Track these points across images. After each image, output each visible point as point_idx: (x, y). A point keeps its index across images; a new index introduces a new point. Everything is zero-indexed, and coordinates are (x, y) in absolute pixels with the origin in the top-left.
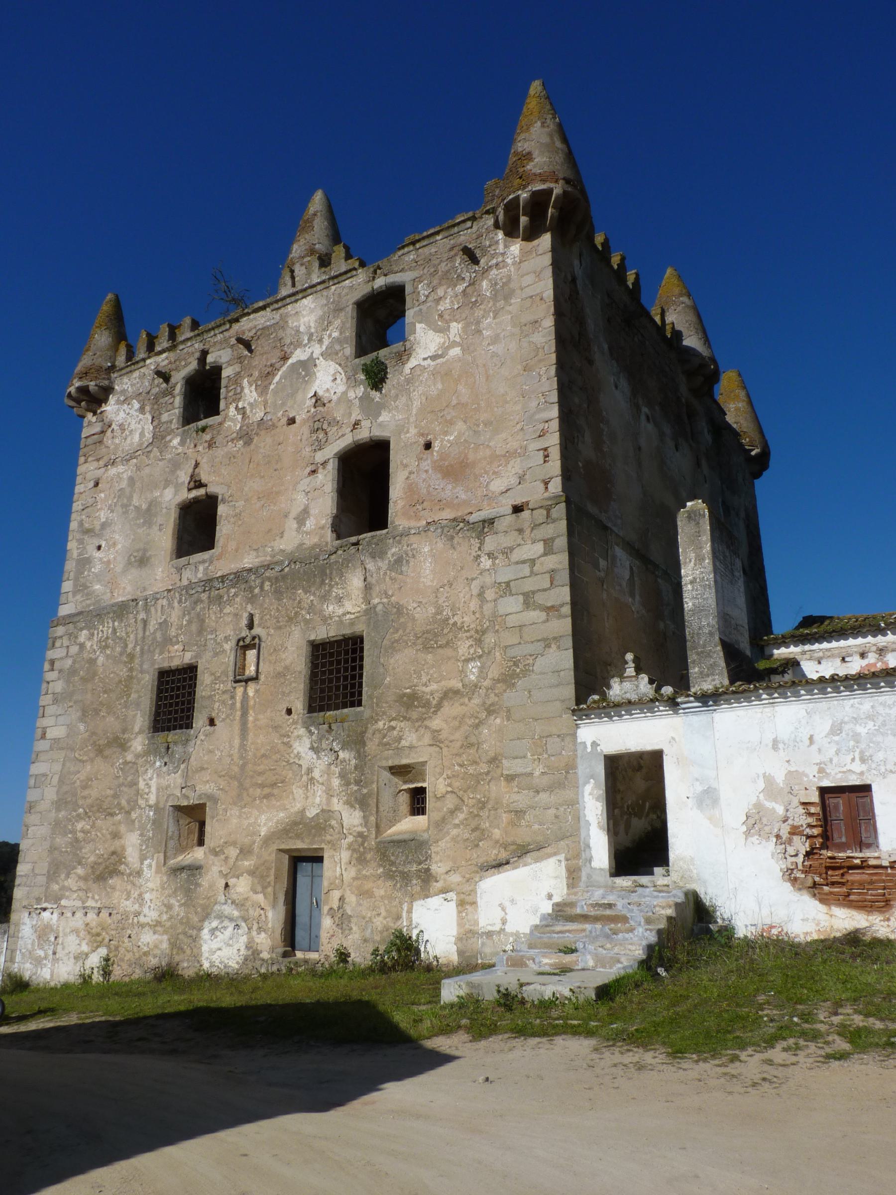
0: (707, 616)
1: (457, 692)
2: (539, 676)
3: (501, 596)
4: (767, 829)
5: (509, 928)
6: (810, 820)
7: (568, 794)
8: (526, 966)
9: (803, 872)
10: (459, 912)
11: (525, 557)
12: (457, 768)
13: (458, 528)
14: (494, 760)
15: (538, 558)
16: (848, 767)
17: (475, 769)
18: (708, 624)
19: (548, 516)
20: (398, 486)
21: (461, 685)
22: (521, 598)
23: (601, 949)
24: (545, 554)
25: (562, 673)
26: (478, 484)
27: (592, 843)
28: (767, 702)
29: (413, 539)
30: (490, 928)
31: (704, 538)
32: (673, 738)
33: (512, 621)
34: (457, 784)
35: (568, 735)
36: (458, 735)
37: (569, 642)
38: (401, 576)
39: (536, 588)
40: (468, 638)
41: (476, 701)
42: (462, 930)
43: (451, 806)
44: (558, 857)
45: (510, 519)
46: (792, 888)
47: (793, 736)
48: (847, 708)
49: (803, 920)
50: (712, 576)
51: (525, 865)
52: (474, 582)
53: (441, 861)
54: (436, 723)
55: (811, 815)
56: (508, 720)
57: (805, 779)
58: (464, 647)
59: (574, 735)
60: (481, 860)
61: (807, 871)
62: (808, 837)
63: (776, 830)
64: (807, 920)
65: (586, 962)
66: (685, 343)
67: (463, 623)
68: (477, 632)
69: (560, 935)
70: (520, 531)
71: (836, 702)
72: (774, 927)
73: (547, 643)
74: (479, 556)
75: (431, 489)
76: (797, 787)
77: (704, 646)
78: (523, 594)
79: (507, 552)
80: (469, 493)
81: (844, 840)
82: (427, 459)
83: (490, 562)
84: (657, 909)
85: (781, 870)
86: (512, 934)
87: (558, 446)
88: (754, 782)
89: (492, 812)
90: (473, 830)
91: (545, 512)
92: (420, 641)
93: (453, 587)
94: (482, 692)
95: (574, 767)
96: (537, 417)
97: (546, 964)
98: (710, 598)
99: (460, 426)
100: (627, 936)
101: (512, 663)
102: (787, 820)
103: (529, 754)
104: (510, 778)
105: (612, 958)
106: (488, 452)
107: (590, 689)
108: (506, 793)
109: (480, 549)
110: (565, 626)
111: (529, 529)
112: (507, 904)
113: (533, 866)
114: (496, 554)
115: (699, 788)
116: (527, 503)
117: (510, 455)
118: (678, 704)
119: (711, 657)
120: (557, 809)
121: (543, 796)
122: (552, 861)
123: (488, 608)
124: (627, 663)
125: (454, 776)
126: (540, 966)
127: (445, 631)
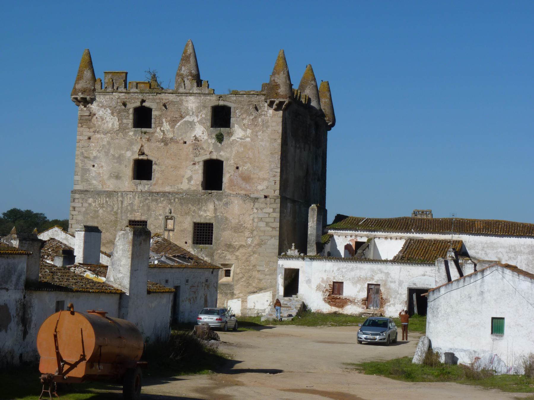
1: (244, 246)
11: (267, 212)
14: (254, 266)
24: (273, 212)
33: (262, 229)
41: (250, 249)
54: (237, 253)
58: (247, 234)
59: (277, 262)
70: (266, 204)
73: (272, 237)
79: (262, 209)
94: (252, 247)
98: (315, 232)
104: (259, 271)
106: (257, 176)
107: (282, 252)
110: (277, 233)
112: (256, 302)
115: (307, 279)
117: (264, 179)
121: (268, 277)
123: (255, 224)
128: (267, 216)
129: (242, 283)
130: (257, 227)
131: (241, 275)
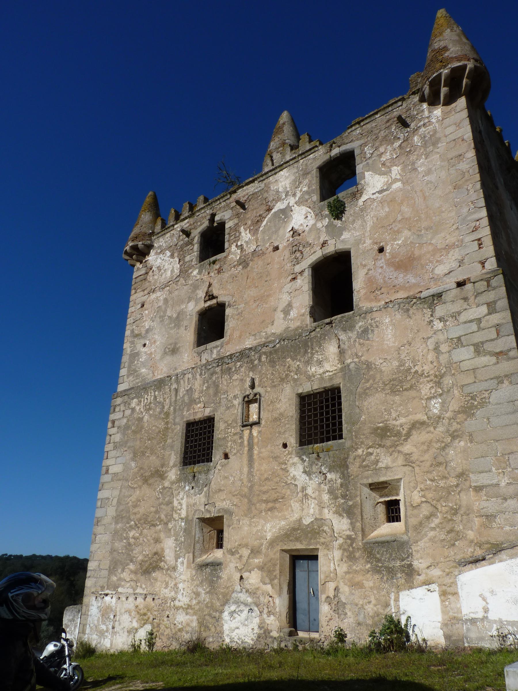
1: (423, 423)
2: (496, 406)
3: (454, 348)
5: (492, 616)
10: (442, 601)
11: (472, 317)
12: (428, 482)
13: (412, 303)
14: (461, 475)
19: (488, 286)
20: (359, 280)
21: (426, 417)
22: (472, 348)
24: (489, 314)
26: (425, 271)
29: (375, 315)
33: (465, 366)
34: (430, 495)
36: (427, 457)
38: (368, 342)
39: (485, 339)
40: (428, 382)
41: (441, 429)
42: (446, 617)
43: (426, 513)
51: (501, 561)
53: (422, 558)
54: (407, 448)
56: (471, 442)
58: (426, 389)
60: (458, 558)
67: (423, 371)
68: (436, 376)
70: (465, 299)
75: (386, 279)
78: (474, 345)
79: (455, 316)
80: (418, 278)
82: (381, 259)
86: (495, 622)
89: (465, 517)
90: (449, 532)
91: (485, 283)
92: (387, 387)
93: (412, 345)
94: (446, 421)
96: (469, 218)
99: (406, 233)
101: (470, 398)
103: (494, 469)
104: (478, 489)
106: (431, 248)
108: (476, 501)
109: (432, 315)
111: (473, 297)
112: (487, 595)
113: (509, 562)
116: (469, 279)
117: (448, 248)
123: (444, 359)
125: (427, 489)
127: (409, 378)
128: (474, 327)
130: (450, 364)
131: (426, 510)
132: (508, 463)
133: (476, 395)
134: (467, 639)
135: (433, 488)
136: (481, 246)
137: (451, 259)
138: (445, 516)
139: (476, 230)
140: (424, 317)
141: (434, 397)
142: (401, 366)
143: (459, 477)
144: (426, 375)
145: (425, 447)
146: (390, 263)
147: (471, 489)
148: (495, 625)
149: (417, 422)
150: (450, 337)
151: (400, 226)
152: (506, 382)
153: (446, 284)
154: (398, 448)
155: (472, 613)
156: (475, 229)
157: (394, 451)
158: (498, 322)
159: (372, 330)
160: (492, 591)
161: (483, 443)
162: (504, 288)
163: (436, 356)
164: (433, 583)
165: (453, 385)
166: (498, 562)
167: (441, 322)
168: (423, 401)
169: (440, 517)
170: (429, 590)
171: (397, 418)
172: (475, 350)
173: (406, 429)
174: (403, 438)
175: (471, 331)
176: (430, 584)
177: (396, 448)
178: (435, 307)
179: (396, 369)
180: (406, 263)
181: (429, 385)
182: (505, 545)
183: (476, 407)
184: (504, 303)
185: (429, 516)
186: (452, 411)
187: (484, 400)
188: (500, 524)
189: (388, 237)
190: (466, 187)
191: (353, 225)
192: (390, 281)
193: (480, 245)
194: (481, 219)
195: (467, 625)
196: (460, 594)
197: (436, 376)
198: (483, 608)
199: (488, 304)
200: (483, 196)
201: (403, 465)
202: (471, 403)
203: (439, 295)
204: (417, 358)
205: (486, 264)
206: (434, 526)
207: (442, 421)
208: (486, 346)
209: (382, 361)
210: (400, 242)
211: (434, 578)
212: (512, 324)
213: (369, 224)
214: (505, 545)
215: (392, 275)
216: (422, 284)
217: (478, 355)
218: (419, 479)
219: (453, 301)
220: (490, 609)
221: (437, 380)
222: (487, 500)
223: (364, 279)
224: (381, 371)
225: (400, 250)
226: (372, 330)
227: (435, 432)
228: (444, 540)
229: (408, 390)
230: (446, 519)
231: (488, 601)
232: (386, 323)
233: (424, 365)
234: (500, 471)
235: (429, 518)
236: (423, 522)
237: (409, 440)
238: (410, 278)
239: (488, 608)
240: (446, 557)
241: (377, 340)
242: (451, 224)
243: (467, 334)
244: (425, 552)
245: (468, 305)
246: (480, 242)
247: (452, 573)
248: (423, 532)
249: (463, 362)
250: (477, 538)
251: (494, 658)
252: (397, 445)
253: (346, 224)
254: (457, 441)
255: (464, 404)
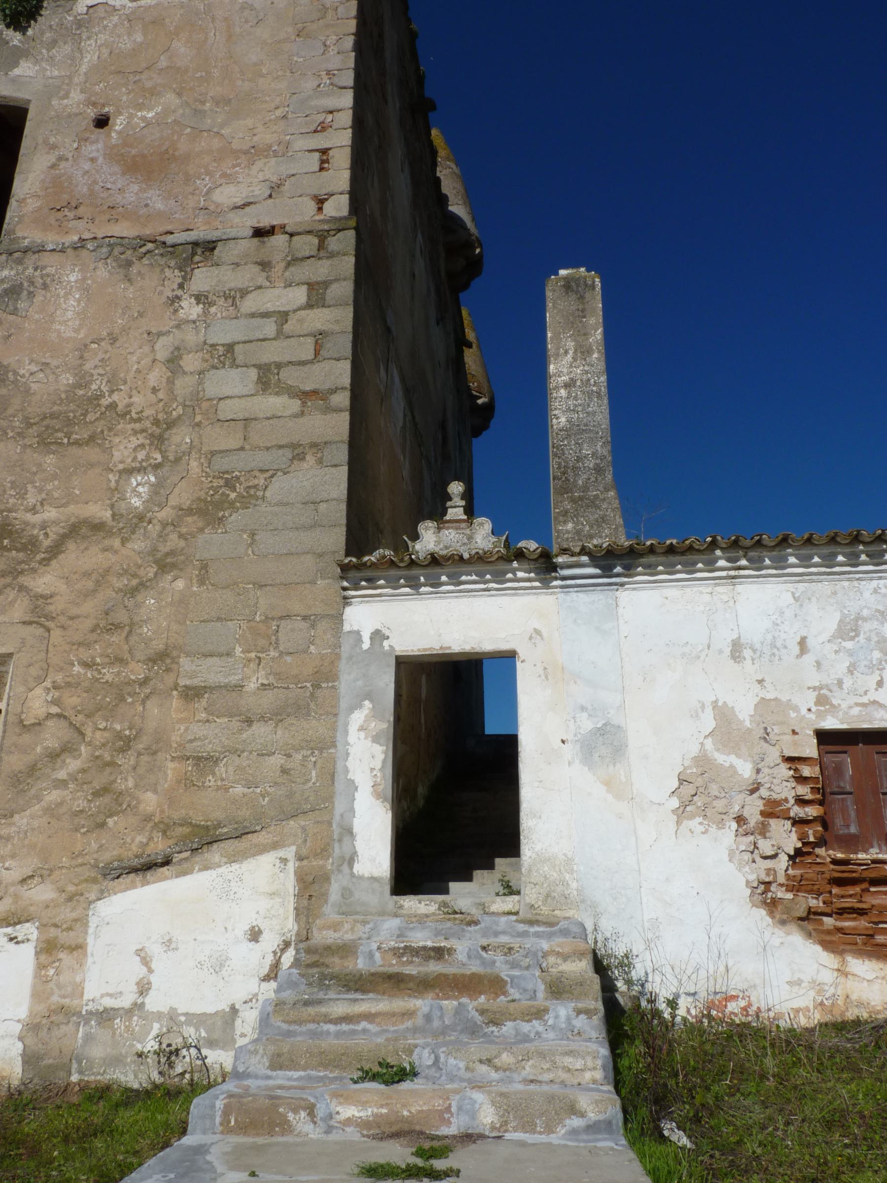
0: (592, 441)
1: (98, 527)
2: (276, 509)
3: (214, 367)
4: (719, 805)
5: (154, 1003)
6: (804, 791)
7: (314, 727)
8: (286, 1127)
9: (790, 889)
10: (40, 967)
11: (270, 307)
12: (77, 669)
13: (143, 250)
14: (162, 658)
15: (295, 311)
16: (872, 696)
17: (118, 674)
18: (593, 454)
19: (321, 247)
20: (31, 176)
21: (109, 514)
22: (253, 373)
23: (484, 1068)
24: (309, 306)
25: (323, 507)
26: (191, 189)
27: (358, 825)
28: (724, 574)
29: (46, 259)
30: (109, 1002)
31: (592, 321)
32: (537, 632)
33: (227, 409)
34: (72, 700)
35: (323, 617)
36: (88, 607)
37: (342, 454)
38: (12, 318)
39: (287, 358)
40: (135, 432)
41: (138, 544)
42: (42, 1008)
43: (53, 743)
44: (281, 853)
45: (250, 245)
46: (769, 920)
47: (769, 637)
48: (867, 595)
49: (789, 983)
50: (603, 378)
51: (206, 868)
52: (161, 338)
53: (13, 856)
54: (45, 581)
55: (801, 779)
56: (202, 582)
57: (793, 715)
58: (125, 448)
59: (339, 618)
60: (106, 856)
61: (796, 886)
62: (797, 822)
63: (737, 808)
64: (799, 983)
65: (473, 1115)
66: (450, 208)
67: (129, 405)
68: (156, 422)
69: (345, 1027)
70: (265, 265)
71: (846, 584)
72: (734, 998)
73: (298, 452)
74: (179, 298)
75: (97, 187)
76: (777, 729)
77: (585, 489)
78: (258, 367)
79: (233, 297)
80: (172, 202)
81: (853, 829)
82: (97, 141)
83: (199, 309)
84: (552, 960)
85: (748, 882)
86: (159, 1016)
87: (348, 150)
88: (696, 716)
89: (145, 758)
90: (97, 794)
91: (316, 241)
92: (33, 431)
93: (118, 344)
94: (154, 529)
95: (332, 676)
96: (313, 103)
97: (348, 1122)
98: (600, 413)
99: (170, 98)
100: (525, 1027)
101: (222, 482)
102: (757, 789)
103: (238, 650)
104: (192, 694)
105: (551, 1099)
106: (216, 143)
107: (377, 537)
108: (180, 721)
109: (181, 286)
110: (338, 425)
111: (283, 264)
112: (155, 949)
113: (223, 870)
114: (211, 298)
115: (587, 725)
116: (283, 227)
117: (255, 153)
118: (554, 568)
119: (598, 507)
120: (289, 756)
121: (260, 731)
122: (266, 863)
123: (184, 386)
124: (450, 499)
125: (68, 685)
126: (329, 1130)
127: (90, 417)
128: (269, 328)
129: (53, 796)
130: (197, 399)
131: (52, 736)
132: (273, 638)
133: (237, 478)
134: (80, 1063)
135: (86, 684)
136: (326, 165)
137: (256, 177)
138: (97, 754)
139: (324, 129)
140: (163, 285)
141: (141, 470)
142: (79, 386)
143: (155, 662)
144: (134, 416)
145: (90, 584)
146: (114, 155)
147: (175, 693)
148: (156, 1026)
149: (85, 522)
150: (209, 342)
151: (159, 81)
152: (310, 459)
153: (232, 227)
154: (22, 579)
155: (108, 995)
156: (322, 128)
157: (9, 585)
158: (323, 328)
159: (30, 293)
160: (170, 941)
161: (227, 587)
162: (352, 260)
163: (168, 378)
164: (28, 921)
165: (192, 446)
166: (200, 870)
167: (198, 304)
168: (111, 476)
169: (84, 754)
170: (11, 939)
171: (38, 507)
172: (259, 378)
173: (52, 536)
174: (39, 557)
175: (261, 337)
176: (19, 923)
177: (15, 578)
178: (193, 270)
179: (66, 392)
180: (149, 164)
181: (134, 441)
182: (225, 830)
183: (232, 504)
184: (344, 289)
185: (58, 750)
186: (173, 508)
187: (252, 492)
188: (223, 780)
189: (125, 98)
190: (323, 38)
191: (48, 50)
192: (104, 195)
193: (323, 162)
194: (339, 111)
195: (87, 1028)
196: (90, 949)
197: (156, 422)
198: (137, 984)
199: (311, 286)
200: (353, 66)
201: (24, 623)
202: (223, 494)
203: (209, 247)
204: (122, 375)
205: (327, 206)
206: (65, 777)
207: (145, 528)
208: (284, 374)
209: (35, 369)
210: (150, 115)
211: (32, 908)
212: (350, 337)
213: (90, 58)
214: (225, 830)
215: (114, 183)
216: (177, 216)
217: (264, 390)
218: (54, 659)
219: (237, 265)
220: (154, 986)
221: (158, 431)
222: (208, 721)
223: (42, 176)
224: (27, 391)
225: (145, 131)
226: (30, 293)
227: (124, 551)
228: (81, 811)
229: (80, 445)
230: (99, 762)
231: (153, 966)
232: (69, 282)
233: (134, 392)
234: (253, 655)
235: (58, 755)
236: (39, 766)
237: (54, 563)
238: (154, 199)
239: (149, 983)
240: (74, 856)
241: (37, 316)
242: (273, 105)
243: (251, 342)
244: (26, 842)
245: (267, 278)
246: (325, 158)
247: (82, 895)
248: (33, 791)
249: (227, 401)
250: (162, 811)
251: (124, 1118)
252: (22, 572)
253: (32, 44)
254: (169, 577)
255: (207, 493)
